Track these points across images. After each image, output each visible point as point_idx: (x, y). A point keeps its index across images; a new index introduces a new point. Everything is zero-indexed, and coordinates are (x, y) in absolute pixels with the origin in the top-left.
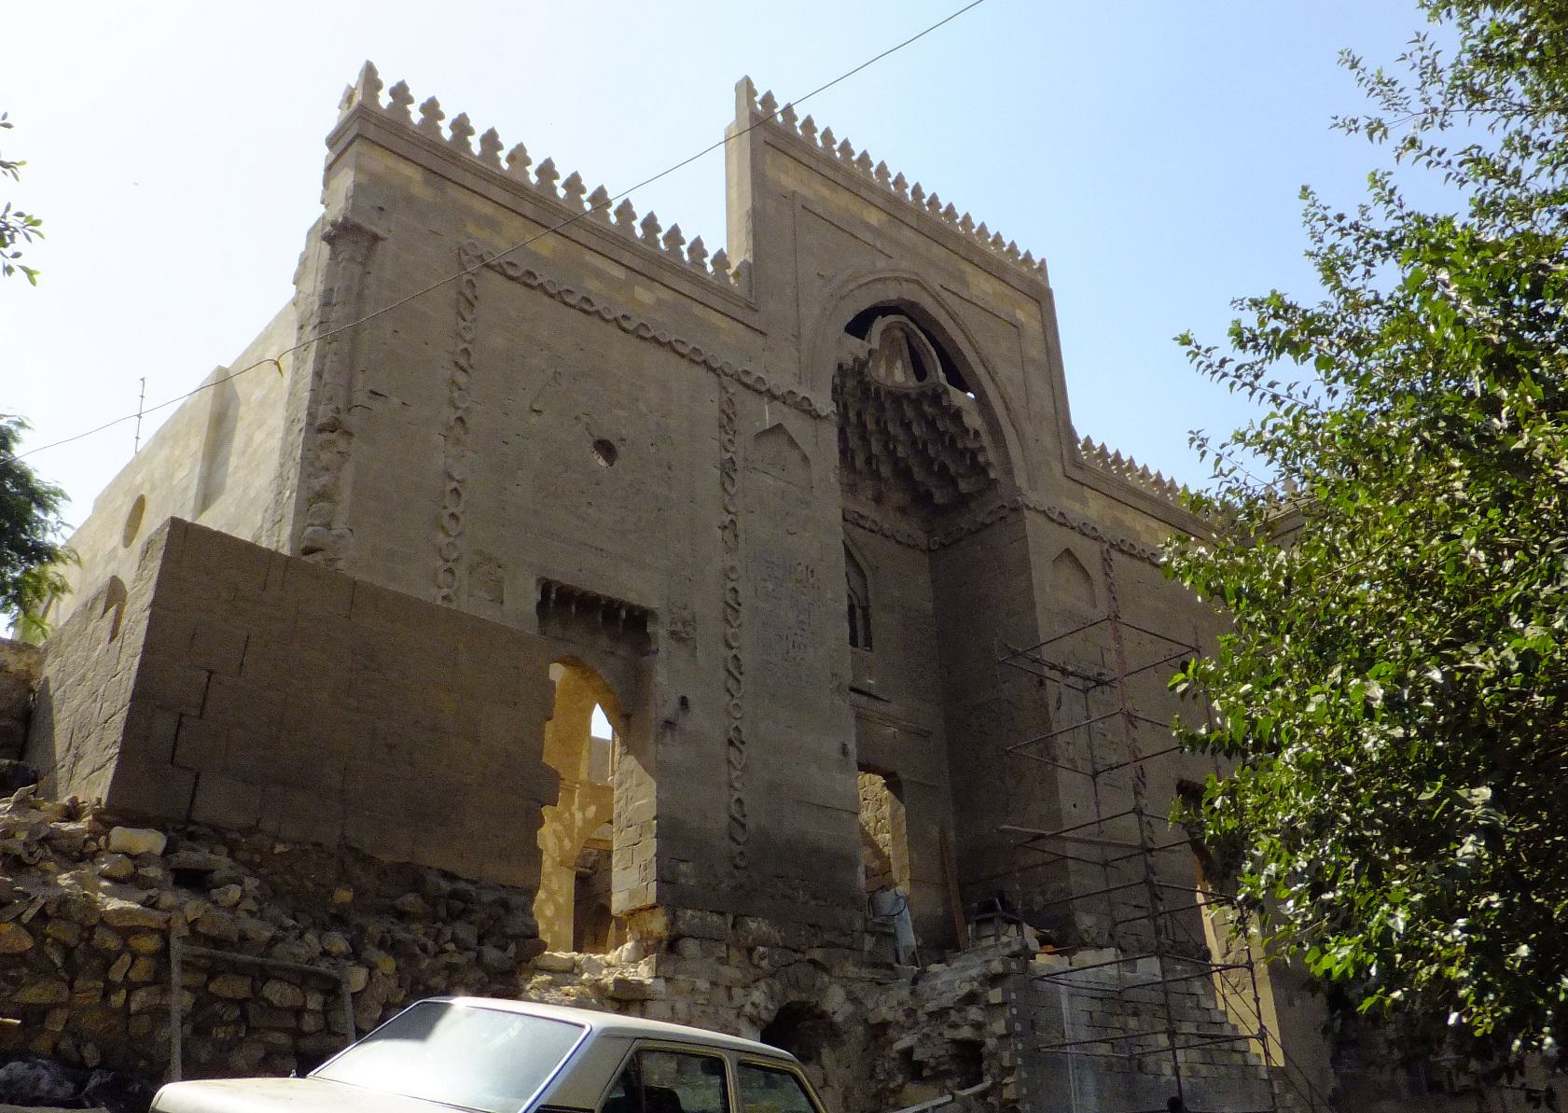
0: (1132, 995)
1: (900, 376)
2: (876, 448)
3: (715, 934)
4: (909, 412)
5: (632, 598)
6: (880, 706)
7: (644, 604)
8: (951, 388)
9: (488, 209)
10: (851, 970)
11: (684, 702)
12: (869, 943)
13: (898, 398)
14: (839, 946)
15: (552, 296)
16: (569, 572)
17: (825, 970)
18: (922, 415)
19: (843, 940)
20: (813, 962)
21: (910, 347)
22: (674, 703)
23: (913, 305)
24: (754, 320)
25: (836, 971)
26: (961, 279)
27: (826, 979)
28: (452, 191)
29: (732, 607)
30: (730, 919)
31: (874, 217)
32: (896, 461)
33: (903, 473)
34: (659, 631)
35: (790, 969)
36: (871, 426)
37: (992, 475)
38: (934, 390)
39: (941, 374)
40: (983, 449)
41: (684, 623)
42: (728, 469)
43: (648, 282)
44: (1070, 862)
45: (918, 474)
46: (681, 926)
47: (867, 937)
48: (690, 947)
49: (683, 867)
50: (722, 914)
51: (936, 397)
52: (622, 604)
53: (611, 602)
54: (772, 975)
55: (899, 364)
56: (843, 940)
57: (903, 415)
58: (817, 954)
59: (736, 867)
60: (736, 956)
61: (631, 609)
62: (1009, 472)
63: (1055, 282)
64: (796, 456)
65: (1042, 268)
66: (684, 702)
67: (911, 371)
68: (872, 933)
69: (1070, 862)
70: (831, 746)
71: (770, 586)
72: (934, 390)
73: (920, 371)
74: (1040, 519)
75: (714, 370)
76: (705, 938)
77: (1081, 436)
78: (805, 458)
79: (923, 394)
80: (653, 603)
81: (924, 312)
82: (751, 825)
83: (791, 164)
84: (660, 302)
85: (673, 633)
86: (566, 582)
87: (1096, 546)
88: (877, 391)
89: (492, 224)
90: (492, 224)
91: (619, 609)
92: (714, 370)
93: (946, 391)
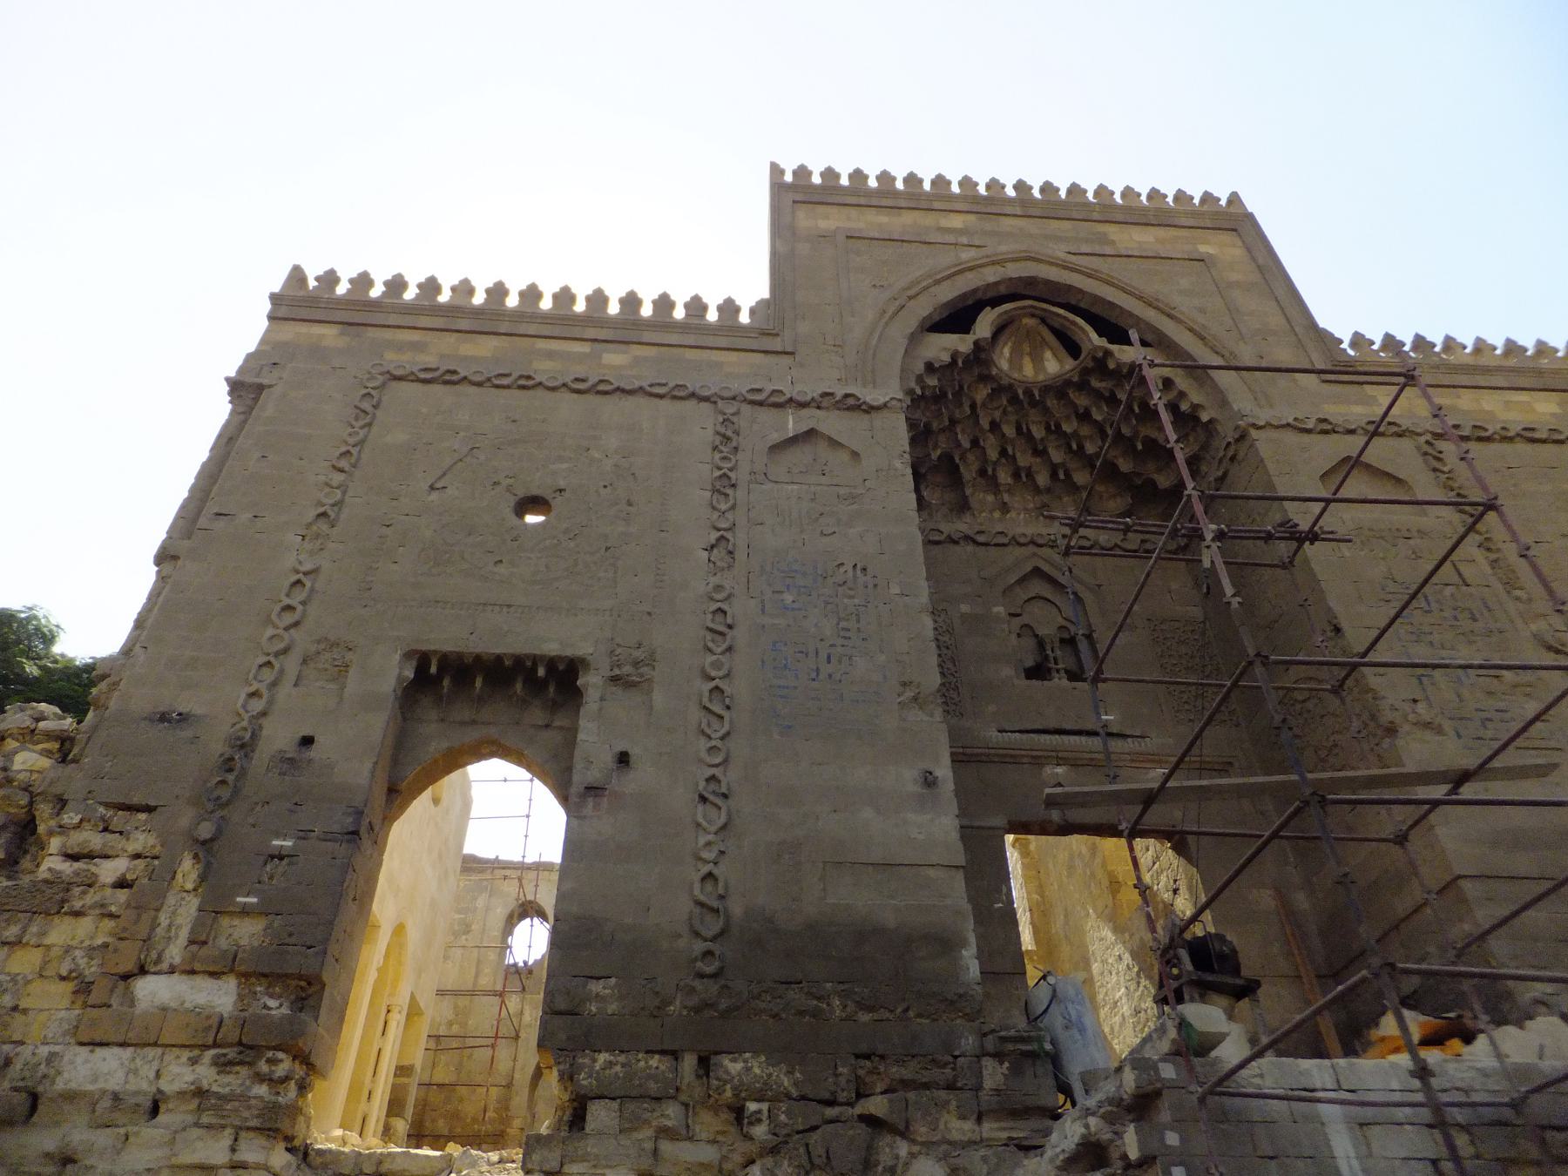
0: (1540, 1106)
1: (1054, 365)
2: (1057, 456)
3: (653, 1087)
4: (1082, 401)
5: (551, 648)
6: (1129, 745)
7: (569, 652)
8: (1114, 348)
9: (415, 336)
10: (960, 1129)
11: (623, 759)
12: (993, 1074)
13: (1059, 389)
14: (926, 1086)
15: (479, 384)
16: (452, 635)
17: (904, 1133)
18: (1098, 394)
19: (936, 1074)
20: (870, 1121)
21: (1053, 330)
22: (607, 758)
23: (1031, 281)
24: (777, 344)
25: (921, 1131)
26: (1104, 239)
27: (903, 1148)
28: (372, 333)
29: (720, 628)
30: (689, 1062)
31: (957, 222)
32: (1089, 462)
33: (1109, 472)
34: (591, 681)
35: (815, 1137)
36: (1038, 432)
37: (1205, 417)
38: (1094, 359)
39: (1094, 335)
40: (1182, 395)
41: (636, 664)
42: (723, 485)
43: (623, 347)
44: (1466, 885)
45: (1125, 466)
46: (584, 1080)
47: (988, 1064)
48: (600, 1115)
49: (596, 987)
50: (675, 1055)
51: (1100, 364)
52: (536, 660)
53: (519, 660)
54: (774, 1151)
55: (1048, 354)
56: (936, 1074)
57: (1075, 406)
58: (877, 1105)
59: (701, 976)
60: (708, 1123)
61: (551, 663)
62: (1224, 403)
63: (1251, 205)
64: (845, 456)
65: (1234, 199)
66: (623, 759)
67: (1063, 353)
68: (999, 1056)
69: (1466, 885)
70: (907, 777)
71: (788, 598)
72: (1094, 359)
73: (1073, 349)
74: (1291, 438)
75: (706, 399)
76: (629, 1096)
77: (1344, 334)
78: (855, 455)
79: (1085, 372)
80: (582, 649)
81: (1047, 282)
82: (736, 908)
83: (835, 209)
84: (637, 361)
85: (615, 679)
86: (448, 647)
87: (1406, 444)
88: (1028, 392)
89: (417, 347)
90: (417, 347)
91: (535, 664)
92: (706, 399)
93: (1108, 353)
